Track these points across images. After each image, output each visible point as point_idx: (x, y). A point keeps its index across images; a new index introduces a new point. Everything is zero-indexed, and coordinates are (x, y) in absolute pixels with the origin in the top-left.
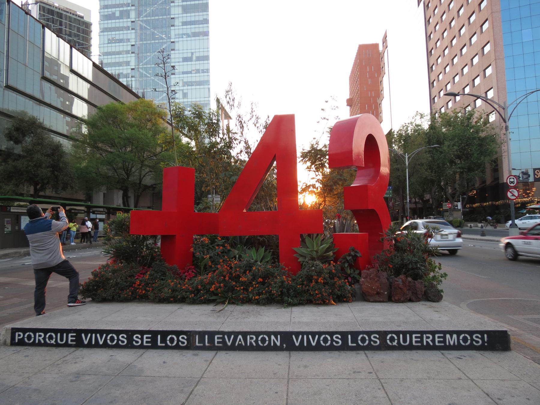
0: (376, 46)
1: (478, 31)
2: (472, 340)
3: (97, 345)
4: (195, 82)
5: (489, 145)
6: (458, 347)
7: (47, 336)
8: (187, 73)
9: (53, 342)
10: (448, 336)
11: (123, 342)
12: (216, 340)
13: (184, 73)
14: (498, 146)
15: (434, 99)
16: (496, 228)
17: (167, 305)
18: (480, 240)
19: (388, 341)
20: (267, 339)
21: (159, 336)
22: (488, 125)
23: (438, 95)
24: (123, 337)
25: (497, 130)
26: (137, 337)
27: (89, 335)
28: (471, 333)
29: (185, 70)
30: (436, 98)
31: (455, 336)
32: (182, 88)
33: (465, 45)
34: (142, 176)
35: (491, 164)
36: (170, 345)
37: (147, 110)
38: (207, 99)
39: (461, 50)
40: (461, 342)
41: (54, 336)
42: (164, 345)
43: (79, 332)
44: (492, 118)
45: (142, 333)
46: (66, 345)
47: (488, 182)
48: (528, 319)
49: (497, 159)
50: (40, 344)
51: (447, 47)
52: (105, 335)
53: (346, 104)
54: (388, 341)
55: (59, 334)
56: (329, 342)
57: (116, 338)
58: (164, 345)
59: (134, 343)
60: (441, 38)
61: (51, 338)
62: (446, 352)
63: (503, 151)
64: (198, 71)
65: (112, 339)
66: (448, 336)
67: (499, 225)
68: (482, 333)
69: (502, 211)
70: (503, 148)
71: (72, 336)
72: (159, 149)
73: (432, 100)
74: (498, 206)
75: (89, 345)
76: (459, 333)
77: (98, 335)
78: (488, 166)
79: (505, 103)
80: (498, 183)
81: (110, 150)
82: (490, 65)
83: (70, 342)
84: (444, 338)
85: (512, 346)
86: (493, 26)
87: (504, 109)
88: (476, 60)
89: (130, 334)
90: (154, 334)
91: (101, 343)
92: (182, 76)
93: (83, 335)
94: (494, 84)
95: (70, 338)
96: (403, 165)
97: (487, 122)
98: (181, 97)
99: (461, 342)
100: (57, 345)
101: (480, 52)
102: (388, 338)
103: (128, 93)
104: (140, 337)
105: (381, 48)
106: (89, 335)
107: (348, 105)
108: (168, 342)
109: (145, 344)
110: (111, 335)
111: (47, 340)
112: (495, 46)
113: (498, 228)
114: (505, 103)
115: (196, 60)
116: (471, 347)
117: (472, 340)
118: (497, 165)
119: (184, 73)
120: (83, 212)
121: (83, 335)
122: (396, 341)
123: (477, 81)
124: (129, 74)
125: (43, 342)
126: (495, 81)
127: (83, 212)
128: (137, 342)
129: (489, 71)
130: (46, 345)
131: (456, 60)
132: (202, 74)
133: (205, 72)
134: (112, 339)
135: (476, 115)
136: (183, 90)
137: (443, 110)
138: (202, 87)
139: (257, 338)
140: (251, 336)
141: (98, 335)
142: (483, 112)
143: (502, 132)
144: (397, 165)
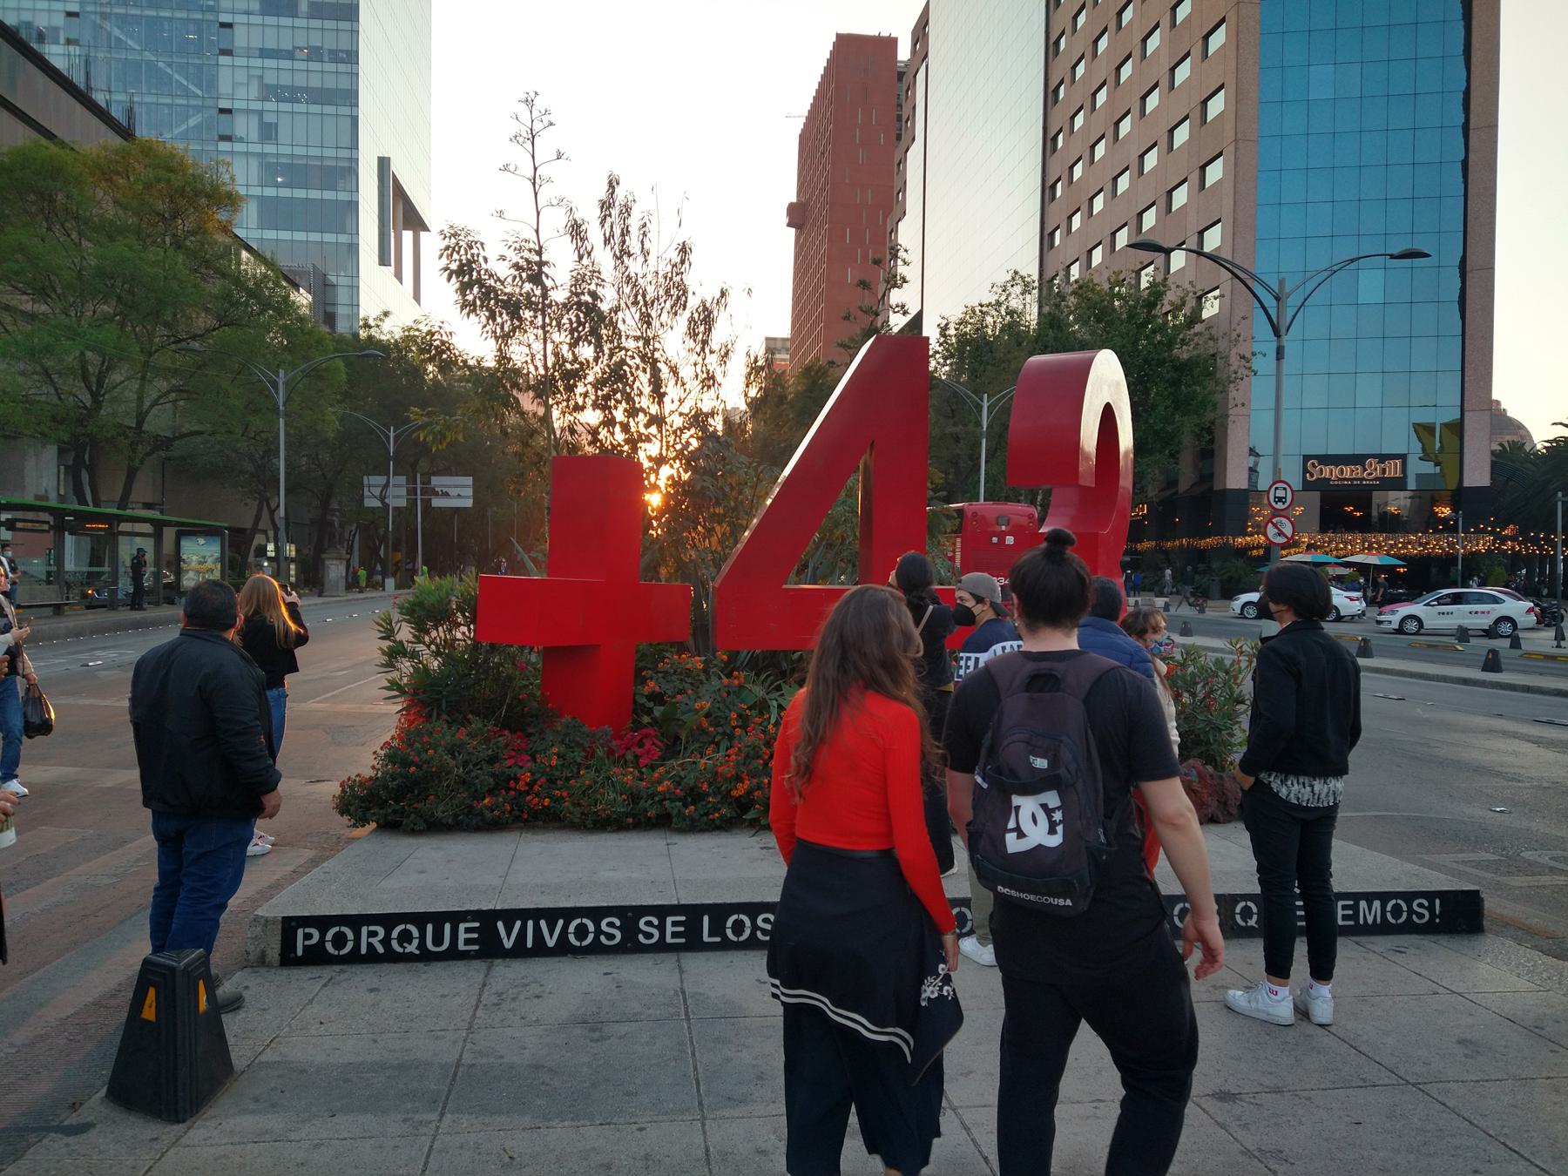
0: (892, 43)
1: (1197, 51)
2: (1411, 911)
3: (540, 950)
4: (307, 89)
5: (1198, 383)
6: (1382, 929)
7: (395, 934)
8: (276, 54)
9: (412, 948)
10: (1363, 904)
11: (611, 937)
12: (1340, 912)
13: (264, 53)
14: (1220, 388)
15: (1052, 234)
16: (1202, 611)
17: (614, 836)
18: (1483, 684)
19: (1238, 918)
20: (350, 935)
21: (706, 919)
22: (1198, 328)
23: (1064, 225)
24: (611, 925)
25: (1223, 345)
26: (649, 924)
27: (518, 924)
28: (1409, 897)
29: (271, 44)
30: (1058, 233)
31: (1377, 904)
32: (257, 106)
33: (1156, 86)
34: (147, 404)
35: (1199, 437)
36: (734, 938)
37: (168, 181)
38: (345, 154)
39: (1144, 98)
40: (1389, 916)
41: (416, 933)
42: (718, 939)
43: (487, 918)
44: (1211, 309)
45: (662, 912)
46: (453, 954)
47: (1184, 486)
48: (1477, 865)
49: (1213, 423)
50: (372, 957)
51: (1104, 84)
52: (561, 922)
53: (785, 220)
54: (1238, 918)
55: (430, 927)
56: (591, 937)
57: (591, 927)
58: (718, 939)
59: (641, 937)
60: (1088, 55)
61: (405, 937)
62: (1362, 939)
63: (1231, 403)
64: (315, 54)
65: (581, 932)
66: (1363, 904)
67: (1210, 603)
68: (1430, 896)
69: (1215, 565)
70: (1233, 394)
71: (468, 930)
72: (203, 321)
73: (1046, 239)
74: (1204, 551)
75: (520, 951)
76: (1384, 897)
77: (543, 923)
78: (1187, 440)
79: (1281, 283)
80: (1211, 488)
81: (28, 307)
82: (1220, 155)
83: (461, 946)
84: (1355, 908)
85: (1486, 923)
86: (1236, 39)
87: (1278, 299)
88: (1182, 135)
89: (629, 915)
90: (693, 913)
91: (551, 943)
92: (257, 62)
93: (500, 925)
94: (1227, 213)
95: (462, 936)
96: (971, 427)
97: (1195, 318)
98: (254, 136)
99: (1389, 916)
100: (425, 957)
101: (1196, 114)
102: (1238, 910)
103: (79, 108)
104: (656, 922)
105: (904, 53)
106: (518, 924)
107: (789, 225)
108: (729, 932)
109: (669, 939)
110: (578, 921)
111: (395, 944)
112: (1237, 102)
113: (1210, 614)
114: (1281, 283)
115: (311, 17)
116: (1409, 928)
117: (1411, 911)
118: (1212, 441)
119: (264, 53)
120: (46, 527)
121: (500, 925)
122: (416, 942)
123: (1180, 197)
124: (56, 29)
125: (381, 950)
126: (1228, 201)
127: (46, 527)
128: (649, 936)
129: (1215, 173)
130: (391, 957)
131: (1125, 127)
132: (331, 67)
133: (343, 61)
134: (581, 932)
135: (1171, 296)
136: (261, 113)
137: (1075, 272)
138: (328, 109)
139: (323, 936)
140: (372, 928)
141: (543, 923)
142: (1189, 288)
143: (1234, 351)
144: (955, 424)
